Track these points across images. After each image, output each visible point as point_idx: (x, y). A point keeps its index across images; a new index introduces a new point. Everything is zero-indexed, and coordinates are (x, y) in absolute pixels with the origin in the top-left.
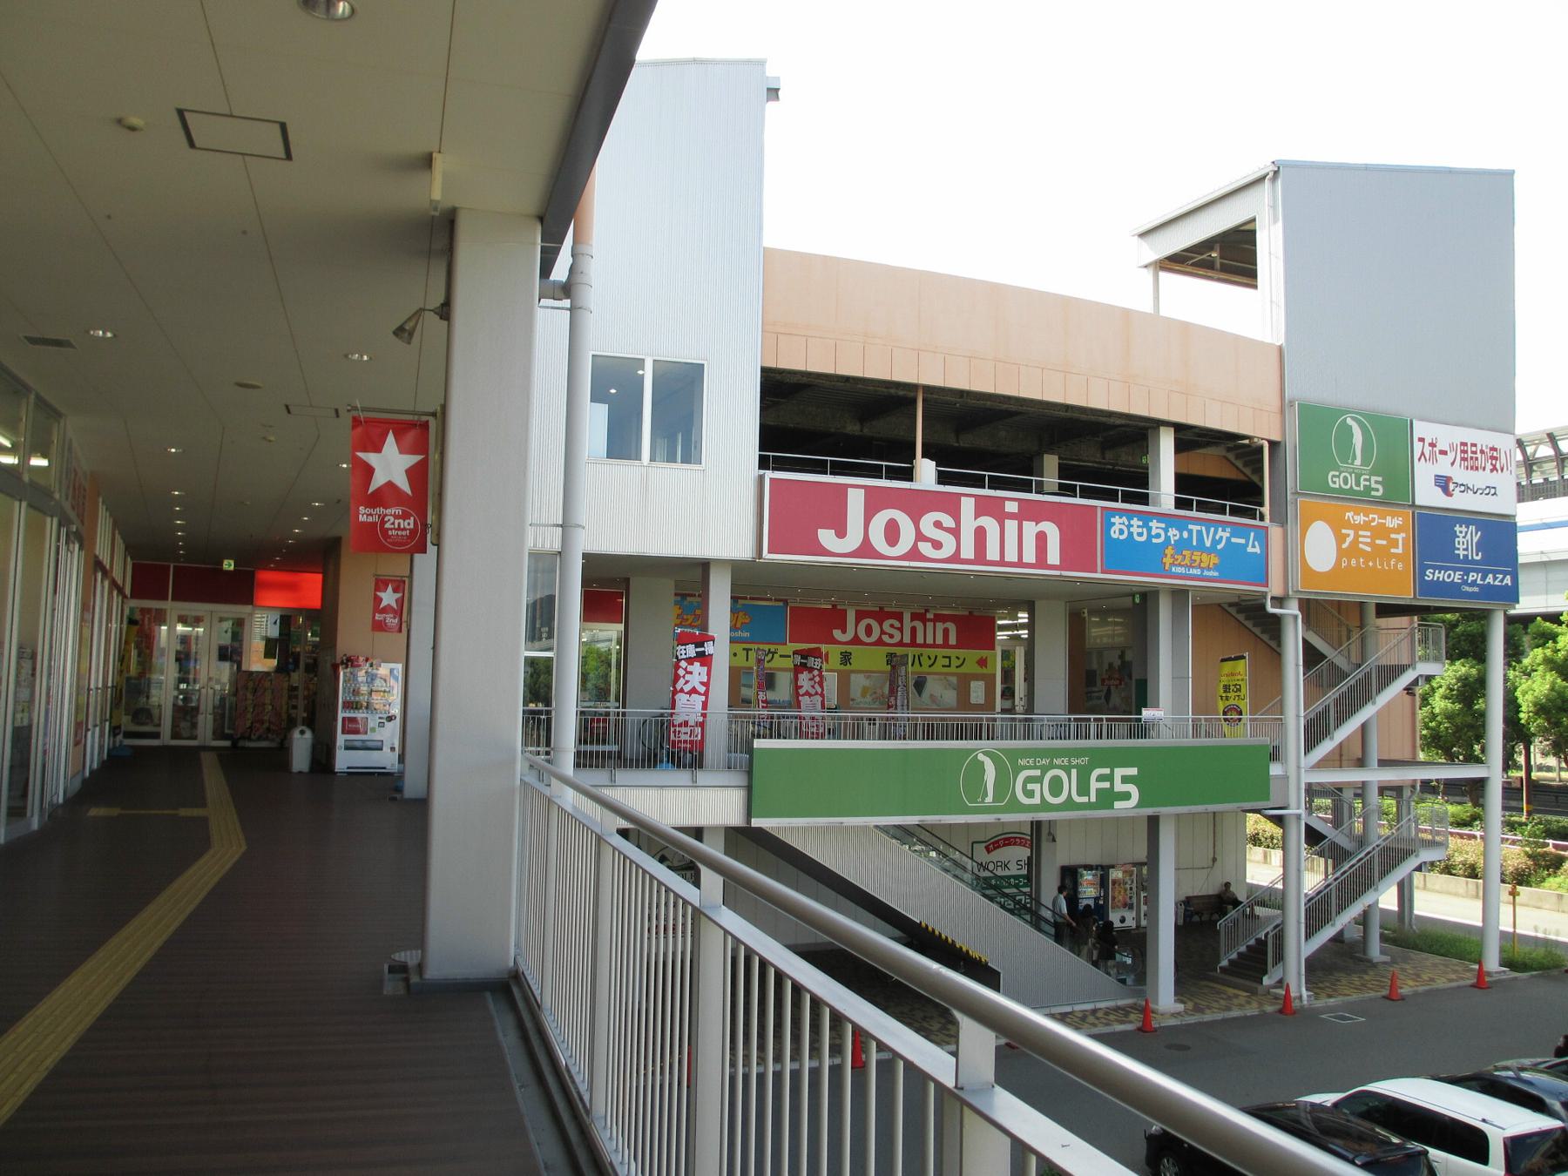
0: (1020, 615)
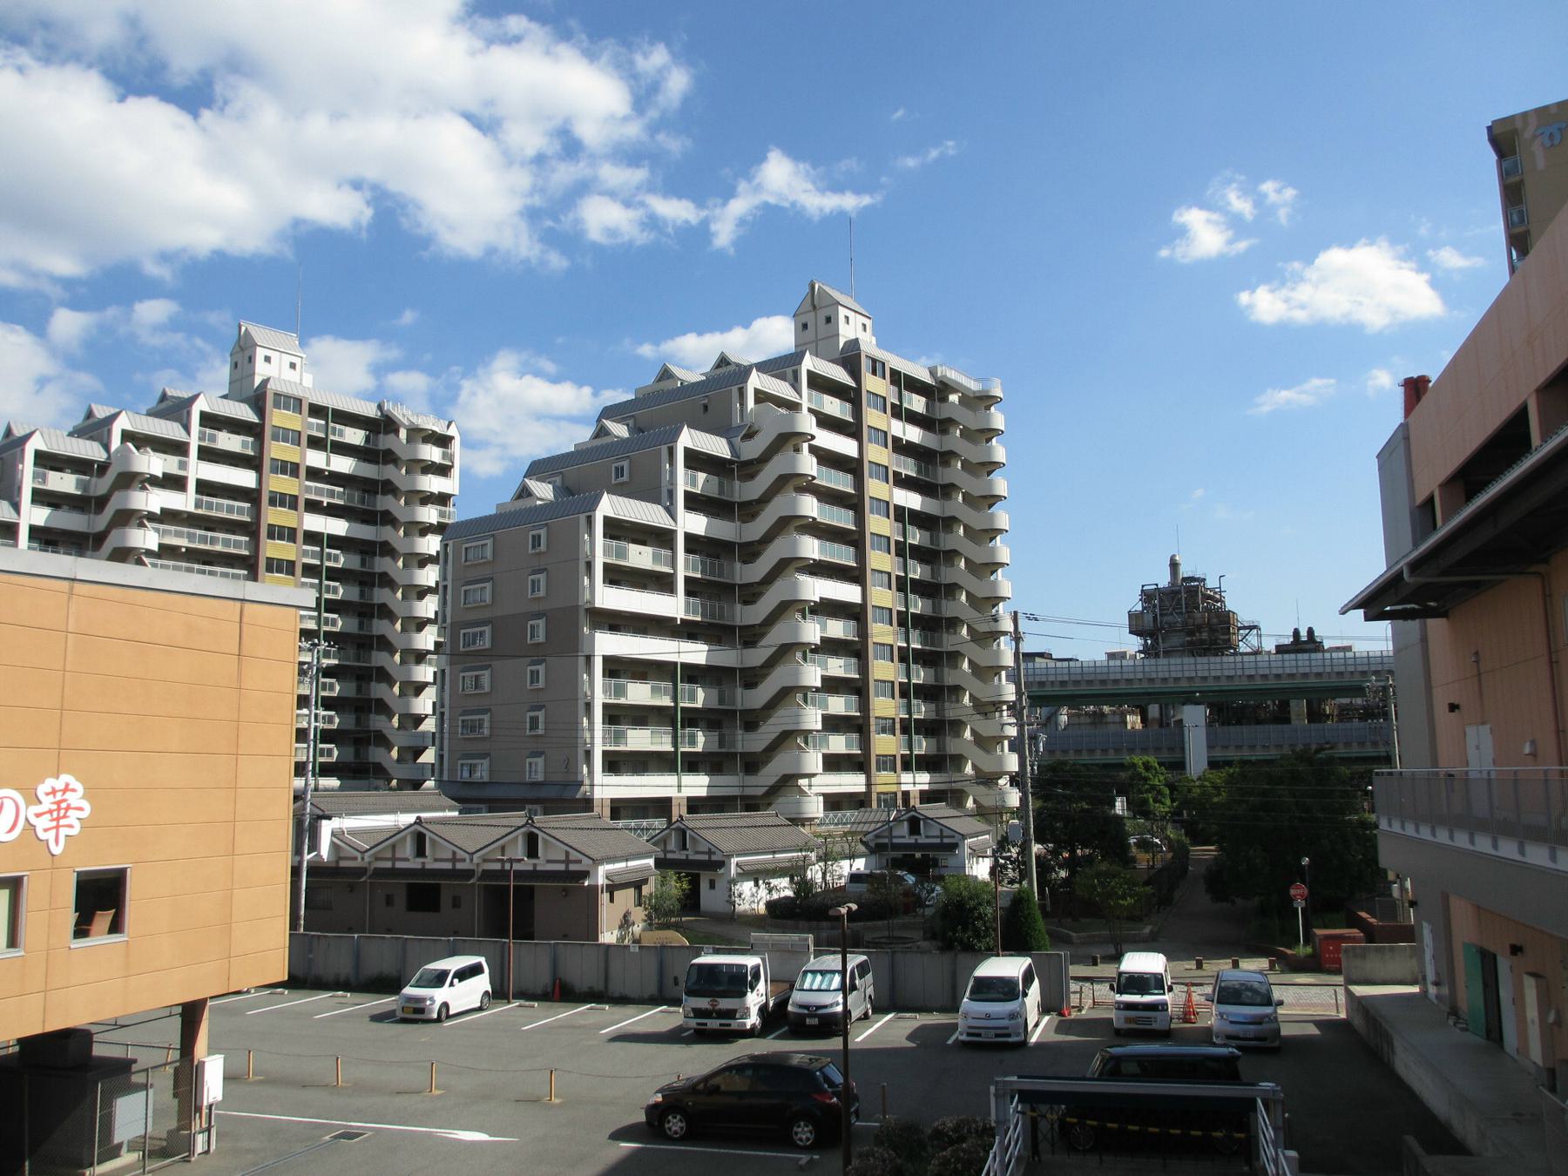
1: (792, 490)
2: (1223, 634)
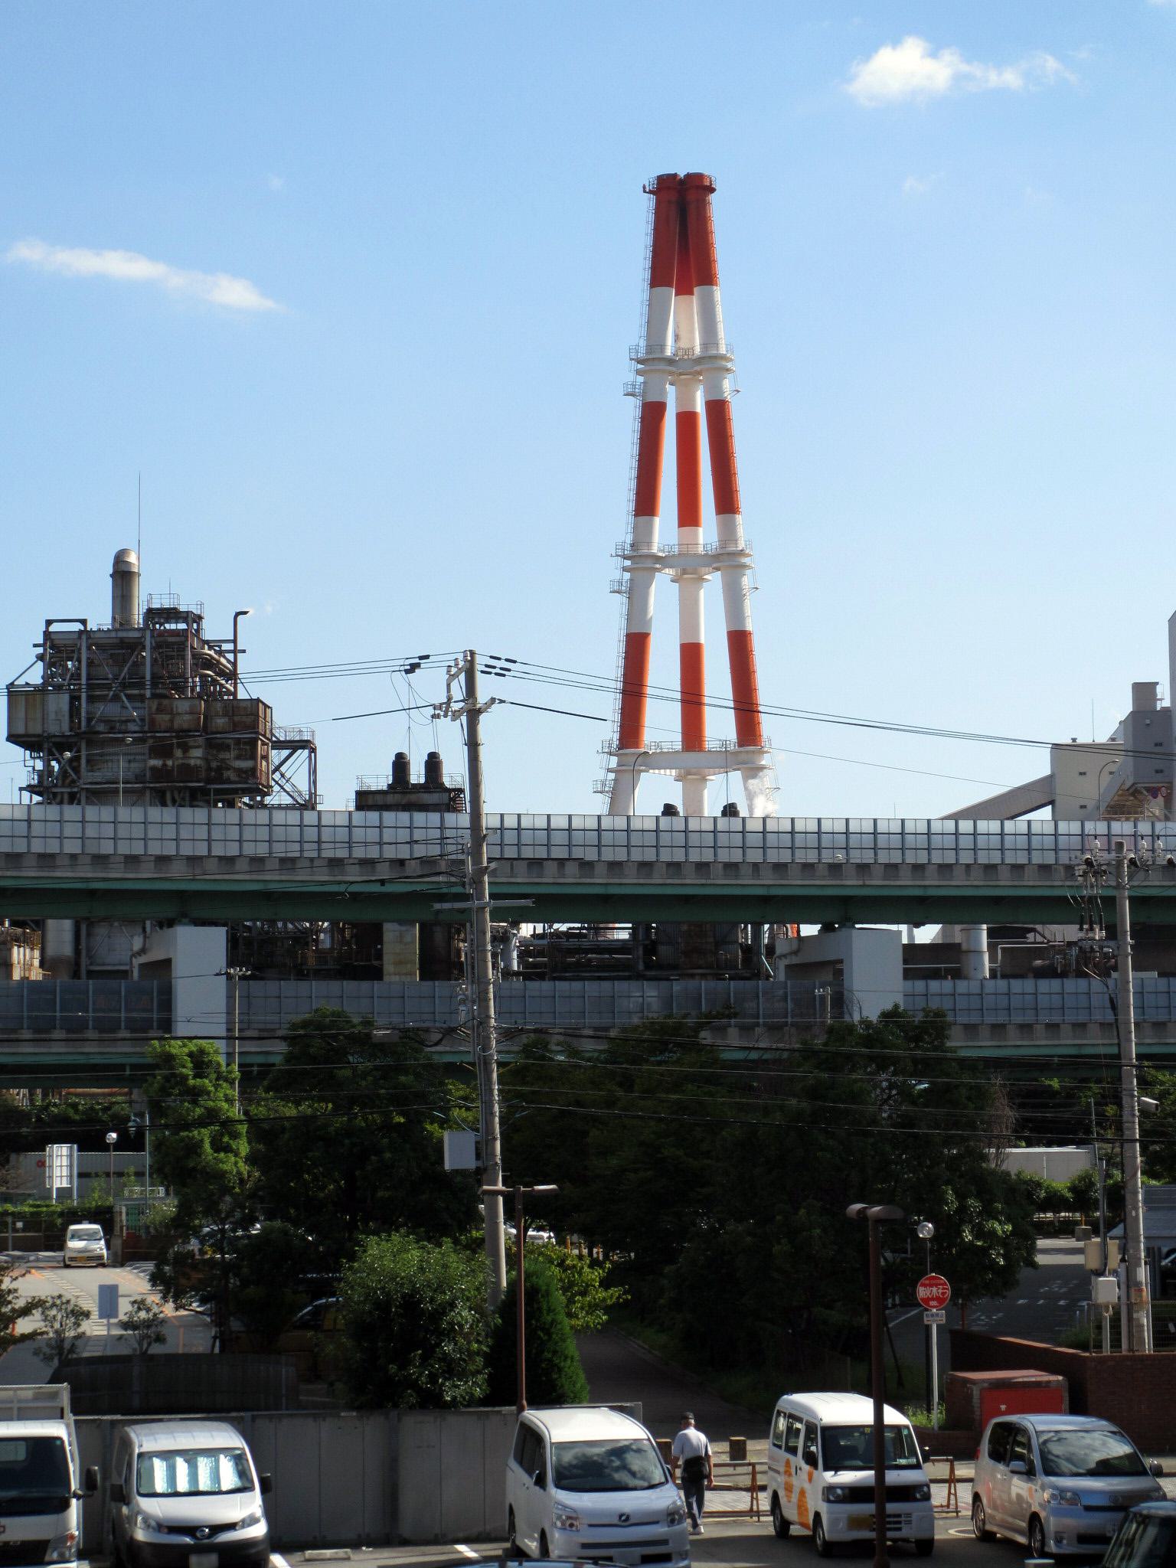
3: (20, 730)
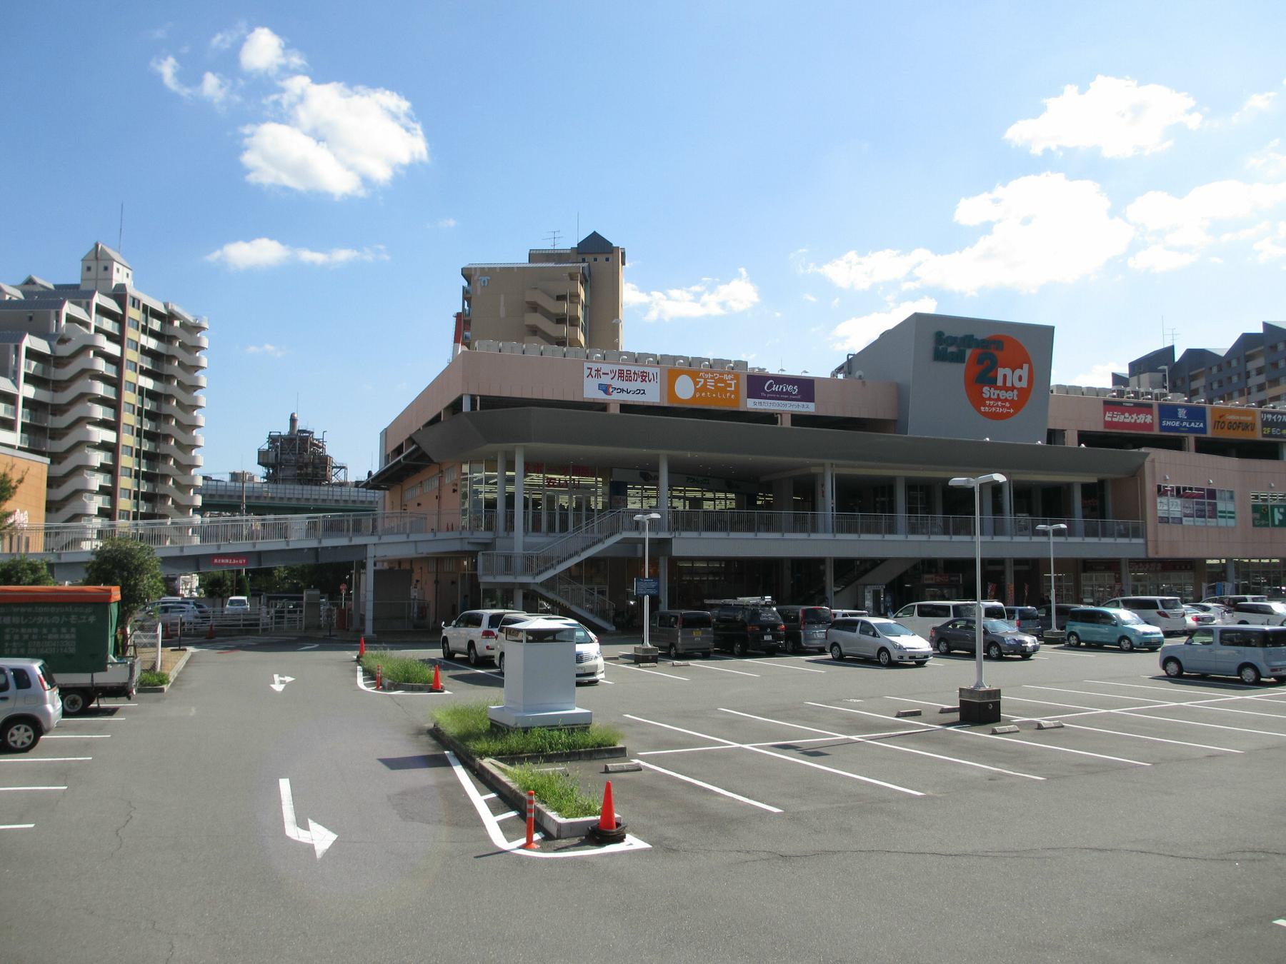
0: (766, 597)
1: (88, 377)
2: (322, 471)
3: (261, 461)
